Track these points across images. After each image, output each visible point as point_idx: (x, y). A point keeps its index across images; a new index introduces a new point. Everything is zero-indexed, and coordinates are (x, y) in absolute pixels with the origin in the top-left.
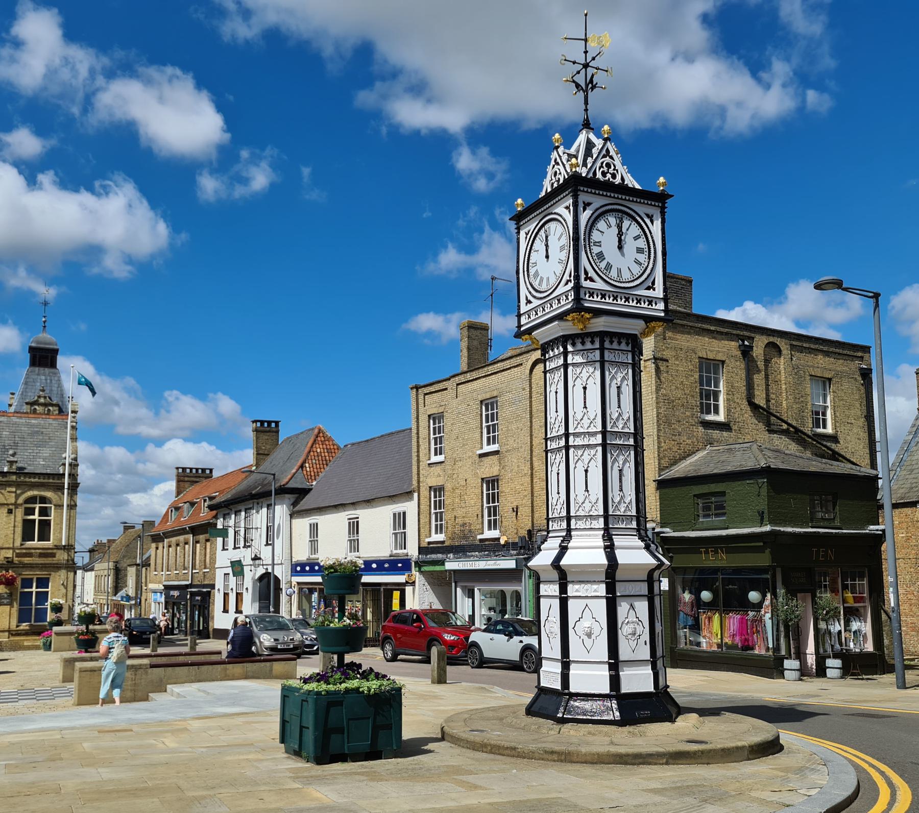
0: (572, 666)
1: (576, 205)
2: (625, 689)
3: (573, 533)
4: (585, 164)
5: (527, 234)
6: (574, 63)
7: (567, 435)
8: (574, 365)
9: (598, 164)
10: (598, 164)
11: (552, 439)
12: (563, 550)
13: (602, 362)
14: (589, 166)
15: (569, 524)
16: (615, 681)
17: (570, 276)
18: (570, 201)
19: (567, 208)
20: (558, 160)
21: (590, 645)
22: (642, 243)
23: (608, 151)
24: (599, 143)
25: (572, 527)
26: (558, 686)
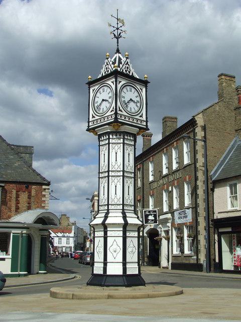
0: (108, 264)
1: (116, 81)
2: (128, 273)
3: (110, 211)
4: (119, 66)
5: (93, 90)
6: (114, 27)
7: (108, 171)
8: (112, 143)
9: (124, 67)
10: (124, 67)
11: (102, 173)
12: (106, 217)
13: (124, 143)
14: (121, 67)
15: (108, 207)
16: (125, 269)
17: (113, 109)
18: (114, 80)
19: (112, 82)
20: (108, 63)
21: (115, 256)
22: (98, 95)
23: (128, 62)
24: (123, 59)
25: (110, 208)
26: (102, 272)
